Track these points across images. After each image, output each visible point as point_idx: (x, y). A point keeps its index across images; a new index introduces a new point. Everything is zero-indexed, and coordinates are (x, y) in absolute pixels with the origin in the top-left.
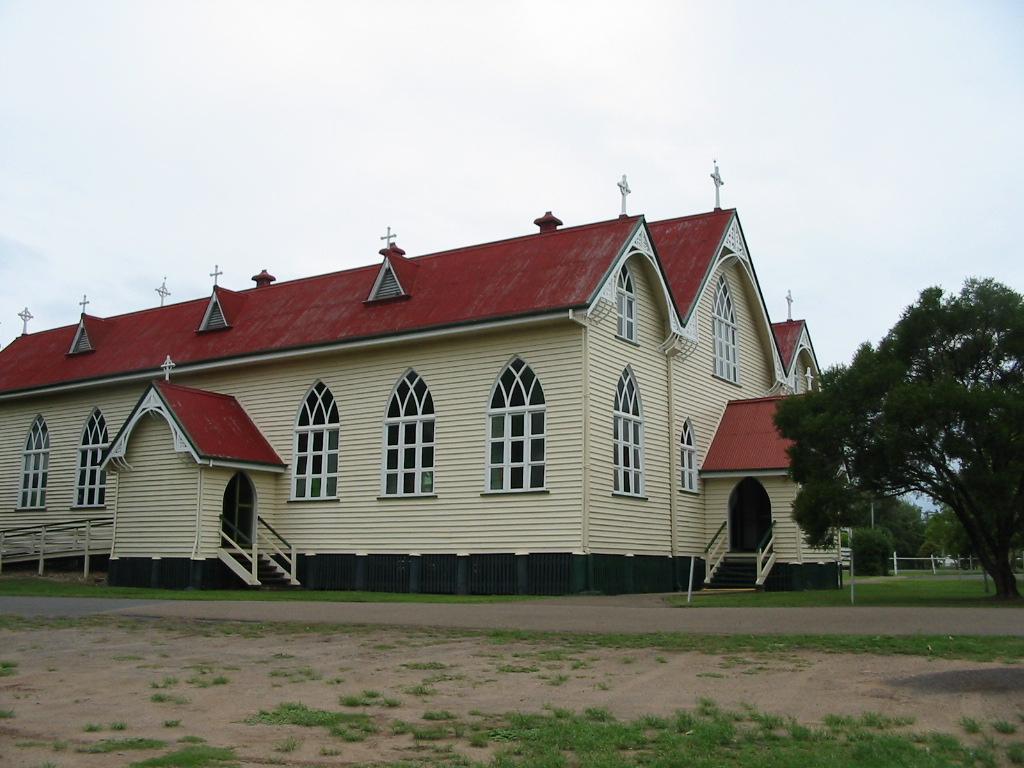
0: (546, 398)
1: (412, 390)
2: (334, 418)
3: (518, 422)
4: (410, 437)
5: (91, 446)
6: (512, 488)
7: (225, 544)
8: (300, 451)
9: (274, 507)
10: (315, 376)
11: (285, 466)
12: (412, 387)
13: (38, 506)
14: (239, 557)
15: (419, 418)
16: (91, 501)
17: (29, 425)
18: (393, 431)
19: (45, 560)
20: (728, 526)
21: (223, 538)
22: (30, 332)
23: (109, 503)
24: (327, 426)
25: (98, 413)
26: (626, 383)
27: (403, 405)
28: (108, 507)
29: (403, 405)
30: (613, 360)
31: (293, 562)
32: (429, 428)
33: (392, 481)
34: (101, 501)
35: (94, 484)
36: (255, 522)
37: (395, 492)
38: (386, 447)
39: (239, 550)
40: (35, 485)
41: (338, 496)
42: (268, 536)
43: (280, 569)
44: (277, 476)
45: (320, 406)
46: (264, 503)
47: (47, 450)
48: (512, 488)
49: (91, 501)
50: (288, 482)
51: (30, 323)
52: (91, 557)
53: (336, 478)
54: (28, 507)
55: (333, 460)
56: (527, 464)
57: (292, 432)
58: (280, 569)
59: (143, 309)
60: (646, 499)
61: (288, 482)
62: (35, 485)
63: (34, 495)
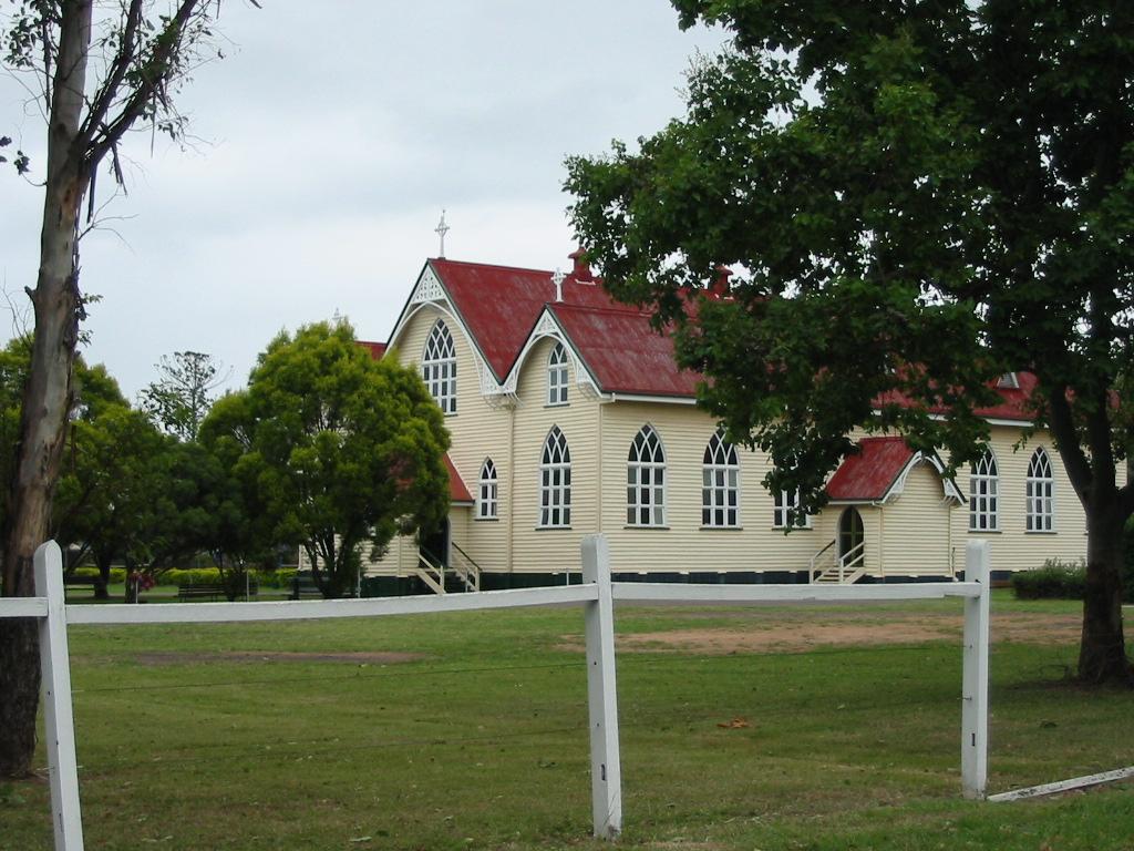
0: (701, 473)
1: (646, 441)
2: (659, 458)
6: (642, 522)
7: (422, 565)
8: (544, 485)
11: (474, 501)
12: (646, 438)
13: (489, 516)
15: (653, 465)
18: (632, 471)
19: (620, 607)
20: (838, 542)
21: (421, 560)
24: (562, 465)
25: (441, 324)
26: (1039, 457)
34: (567, 521)
35: (548, 485)
36: (450, 547)
37: (648, 522)
38: (626, 485)
39: (433, 569)
40: (557, 482)
41: (737, 525)
42: (461, 560)
44: (468, 509)
55: (632, 499)
56: (713, 507)
60: (811, 529)
62: (557, 482)
63: (557, 493)
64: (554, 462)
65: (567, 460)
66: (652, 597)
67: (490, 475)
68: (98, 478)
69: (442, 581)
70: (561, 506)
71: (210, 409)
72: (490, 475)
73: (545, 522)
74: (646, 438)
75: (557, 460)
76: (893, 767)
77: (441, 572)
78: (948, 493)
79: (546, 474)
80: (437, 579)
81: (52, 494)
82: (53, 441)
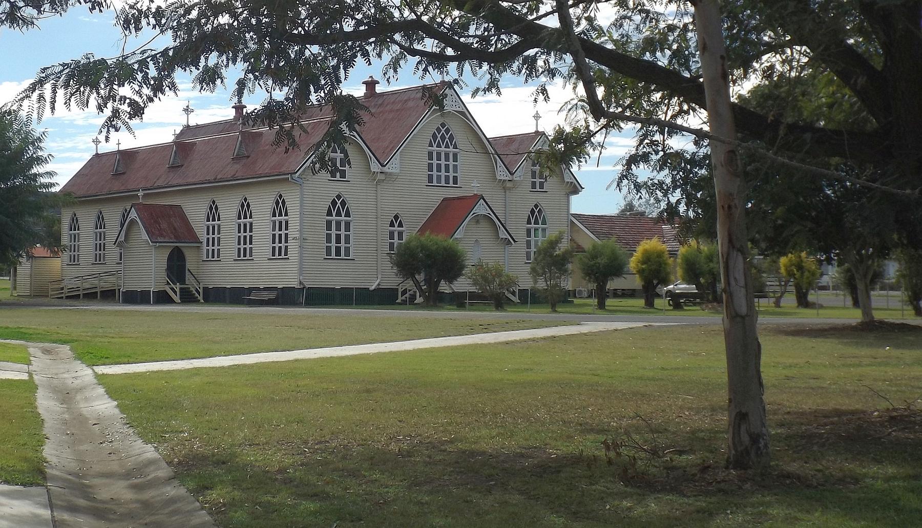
2: (348, 214)
3: (338, 224)
4: (338, 228)
5: (242, 220)
6: (336, 256)
9: (196, 263)
10: (243, 194)
12: (339, 202)
14: (172, 289)
16: (280, 254)
17: (207, 205)
18: (329, 224)
22: (192, 123)
23: (222, 258)
25: (281, 196)
27: (343, 211)
28: (81, 264)
29: (343, 211)
30: (196, 211)
31: (201, 291)
32: (348, 225)
33: (329, 250)
36: (187, 271)
38: (351, 233)
43: (197, 295)
45: (213, 212)
46: (191, 262)
47: (105, 230)
48: (336, 256)
49: (280, 254)
50: (202, 253)
51: (191, 115)
52: (101, 292)
53: (287, 246)
54: (242, 258)
57: (203, 225)
58: (197, 295)
59: (584, 89)
61: (202, 253)
64: (218, 221)
65: (286, 215)
66: (437, 345)
67: (533, 222)
68: (638, 464)
69: (178, 293)
70: (277, 245)
71: (482, 34)
72: (533, 222)
73: (274, 255)
74: (339, 202)
75: (280, 215)
76: (471, 490)
77: (177, 287)
78: (501, 236)
79: (239, 225)
80: (175, 292)
81: (56, 222)
82: (98, 497)
